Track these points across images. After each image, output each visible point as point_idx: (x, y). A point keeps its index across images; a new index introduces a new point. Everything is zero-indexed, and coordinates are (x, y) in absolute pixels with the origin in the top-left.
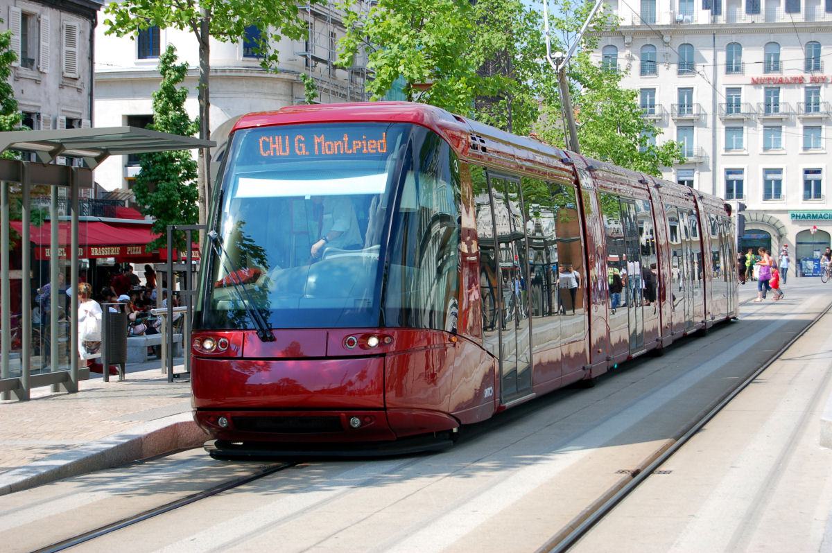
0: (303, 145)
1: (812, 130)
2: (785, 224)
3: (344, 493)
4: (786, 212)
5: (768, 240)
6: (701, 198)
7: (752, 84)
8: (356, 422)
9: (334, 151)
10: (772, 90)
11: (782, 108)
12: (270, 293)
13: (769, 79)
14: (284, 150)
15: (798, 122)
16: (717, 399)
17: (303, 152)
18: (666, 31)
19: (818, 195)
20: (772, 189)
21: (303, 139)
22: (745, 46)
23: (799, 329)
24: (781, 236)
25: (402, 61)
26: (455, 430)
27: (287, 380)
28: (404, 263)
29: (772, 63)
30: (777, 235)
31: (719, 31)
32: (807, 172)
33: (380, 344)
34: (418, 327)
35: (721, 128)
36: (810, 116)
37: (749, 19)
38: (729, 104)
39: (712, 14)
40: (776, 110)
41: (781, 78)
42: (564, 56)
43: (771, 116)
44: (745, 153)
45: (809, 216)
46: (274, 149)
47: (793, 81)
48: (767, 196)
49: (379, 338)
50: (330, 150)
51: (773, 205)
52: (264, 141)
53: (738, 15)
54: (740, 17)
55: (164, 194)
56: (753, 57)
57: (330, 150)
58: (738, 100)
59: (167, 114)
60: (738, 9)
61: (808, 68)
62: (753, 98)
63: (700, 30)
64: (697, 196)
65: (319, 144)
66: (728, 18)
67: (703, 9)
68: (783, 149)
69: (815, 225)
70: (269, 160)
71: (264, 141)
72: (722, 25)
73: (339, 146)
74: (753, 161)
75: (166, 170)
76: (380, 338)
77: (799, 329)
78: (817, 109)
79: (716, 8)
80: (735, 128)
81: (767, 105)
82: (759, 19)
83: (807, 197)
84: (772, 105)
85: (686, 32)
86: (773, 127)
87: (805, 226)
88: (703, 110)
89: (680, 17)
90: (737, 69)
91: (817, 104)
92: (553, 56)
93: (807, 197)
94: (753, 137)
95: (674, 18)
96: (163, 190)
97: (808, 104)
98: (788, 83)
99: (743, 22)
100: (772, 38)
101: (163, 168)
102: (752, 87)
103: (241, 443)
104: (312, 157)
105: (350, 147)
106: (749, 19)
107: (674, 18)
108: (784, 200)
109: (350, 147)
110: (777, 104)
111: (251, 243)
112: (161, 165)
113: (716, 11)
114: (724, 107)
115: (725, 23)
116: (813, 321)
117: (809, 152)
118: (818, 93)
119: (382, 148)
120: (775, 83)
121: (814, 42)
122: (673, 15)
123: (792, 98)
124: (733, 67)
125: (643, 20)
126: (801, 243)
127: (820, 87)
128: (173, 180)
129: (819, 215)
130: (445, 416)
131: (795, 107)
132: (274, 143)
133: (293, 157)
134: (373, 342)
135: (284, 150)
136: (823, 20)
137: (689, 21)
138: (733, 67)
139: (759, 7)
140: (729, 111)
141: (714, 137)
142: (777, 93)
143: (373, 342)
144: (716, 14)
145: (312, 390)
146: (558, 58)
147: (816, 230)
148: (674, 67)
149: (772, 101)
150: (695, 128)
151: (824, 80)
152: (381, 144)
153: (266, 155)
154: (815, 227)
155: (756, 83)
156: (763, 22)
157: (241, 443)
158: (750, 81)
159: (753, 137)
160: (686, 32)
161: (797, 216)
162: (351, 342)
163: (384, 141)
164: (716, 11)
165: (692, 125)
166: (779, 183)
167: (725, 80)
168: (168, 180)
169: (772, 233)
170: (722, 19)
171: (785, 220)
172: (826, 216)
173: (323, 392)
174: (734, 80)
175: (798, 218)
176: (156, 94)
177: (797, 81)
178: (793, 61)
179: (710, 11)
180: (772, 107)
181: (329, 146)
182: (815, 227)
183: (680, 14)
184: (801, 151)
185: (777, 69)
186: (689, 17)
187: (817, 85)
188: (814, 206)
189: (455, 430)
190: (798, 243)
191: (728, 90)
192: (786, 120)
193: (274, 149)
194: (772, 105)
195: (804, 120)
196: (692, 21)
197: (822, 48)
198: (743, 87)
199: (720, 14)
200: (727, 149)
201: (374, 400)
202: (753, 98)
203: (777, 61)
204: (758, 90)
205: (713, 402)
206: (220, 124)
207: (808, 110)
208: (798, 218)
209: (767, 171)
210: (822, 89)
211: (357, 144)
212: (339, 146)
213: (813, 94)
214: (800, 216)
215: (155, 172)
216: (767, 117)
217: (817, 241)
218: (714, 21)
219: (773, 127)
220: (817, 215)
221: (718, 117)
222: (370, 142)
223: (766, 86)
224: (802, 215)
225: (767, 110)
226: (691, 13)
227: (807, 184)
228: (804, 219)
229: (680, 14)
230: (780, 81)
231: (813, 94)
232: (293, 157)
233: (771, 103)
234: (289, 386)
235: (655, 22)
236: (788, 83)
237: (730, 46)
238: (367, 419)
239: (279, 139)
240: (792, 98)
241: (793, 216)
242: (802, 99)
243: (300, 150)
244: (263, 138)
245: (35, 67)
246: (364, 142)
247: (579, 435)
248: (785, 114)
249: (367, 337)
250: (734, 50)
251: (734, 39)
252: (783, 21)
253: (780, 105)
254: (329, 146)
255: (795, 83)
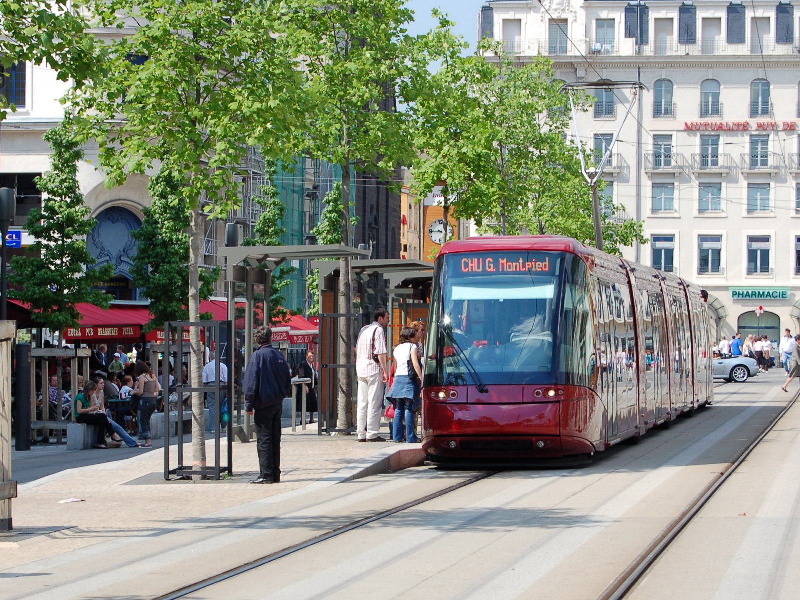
0: (492, 265)
1: (759, 188)
2: (725, 304)
3: (554, 482)
4: (726, 288)
6: (633, 270)
7: (685, 131)
8: (541, 444)
9: (513, 269)
10: (710, 139)
11: (721, 161)
13: (706, 125)
14: (479, 268)
15: (741, 178)
16: (743, 449)
17: (492, 270)
18: (580, 63)
19: (765, 268)
20: (709, 261)
21: (492, 261)
22: (678, 84)
23: (770, 418)
24: (720, 319)
25: (446, 170)
26: (592, 454)
27: (485, 417)
28: (566, 344)
29: (711, 106)
30: (714, 317)
31: (646, 65)
32: (752, 239)
33: (557, 395)
34: (574, 385)
35: (647, 184)
36: (756, 171)
37: (682, 50)
38: (657, 156)
39: (637, 44)
40: (715, 163)
41: (721, 124)
42: (597, 171)
43: (708, 171)
44: (677, 215)
45: (754, 294)
46: (472, 267)
47: (735, 128)
49: (555, 391)
50: (510, 268)
51: (709, 280)
52: (465, 262)
53: (668, 45)
54: (672, 49)
55: (166, 276)
56: (687, 101)
57: (510, 268)
58: (668, 150)
59: (166, 198)
60: (669, 38)
61: (754, 113)
62: (687, 148)
63: (623, 63)
64: (629, 269)
65: (503, 265)
66: (656, 49)
67: (626, 37)
68: (723, 211)
69: (761, 305)
70: (467, 274)
71: (465, 262)
72: (649, 58)
73: (516, 266)
74: (684, 223)
75: (167, 253)
76: (557, 391)
77: (770, 418)
78: (765, 163)
79: (641, 36)
80: (664, 185)
81: (704, 156)
82: (695, 50)
83: (751, 271)
84: (710, 156)
85: (606, 66)
86: (711, 187)
87: (748, 306)
88: (625, 161)
89: (598, 47)
90: (667, 112)
91: (765, 155)
92: (587, 171)
93: (751, 271)
94: (687, 195)
95: (591, 48)
96: (166, 273)
97: (754, 156)
98: (730, 130)
99: (674, 54)
100: (711, 74)
101: (164, 251)
102: (685, 134)
104: (498, 273)
105: (524, 266)
106: (682, 50)
107: (591, 48)
108: (723, 274)
109: (524, 266)
110: (715, 156)
112: (162, 248)
113: (642, 40)
114: (651, 158)
115: (652, 54)
116: (786, 408)
117: (755, 215)
118: (766, 143)
119: (546, 267)
120: (713, 130)
121: (762, 79)
122: (589, 44)
123: (733, 150)
124: (661, 110)
125: (552, 49)
126: (744, 328)
127: (769, 136)
128: (174, 263)
129: (766, 293)
130: (589, 444)
131: (738, 160)
132: (472, 263)
133: (485, 273)
134: (552, 393)
135: (479, 268)
136: (774, 54)
137: (608, 52)
138: (661, 110)
139: (695, 36)
140: (657, 164)
141: (639, 195)
142: (716, 143)
143: (552, 393)
144: (642, 43)
145: (501, 424)
146: (592, 173)
147: (762, 312)
148: (591, 110)
149: (710, 152)
150: (615, 184)
151: (774, 127)
152: (546, 265)
153: (466, 271)
154: (761, 308)
155: (690, 129)
156: (700, 54)
158: (683, 128)
159: (687, 195)
160: (606, 66)
161: (739, 294)
162: (538, 394)
163: (547, 264)
164: (642, 40)
165: (611, 180)
166: (718, 253)
167: (654, 125)
168: (169, 263)
170: (649, 50)
171: (725, 299)
172: (775, 295)
173: (507, 425)
174: (663, 125)
175: (741, 296)
176: (154, 178)
177: (741, 128)
178: (735, 103)
179: (634, 39)
180: (710, 159)
181: (510, 266)
182: (761, 308)
183: (597, 42)
184: (745, 214)
185: (716, 112)
186: (607, 47)
187: (765, 133)
188: (759, 282)
189: (592, 454)
190: (739, 328)
191: (656, 137)
192: (727, 175)
193: (472, 267)
194: (710, 156)
195: (748, 176)
196: (613, 52)
197: (772, 87)
198: (674, 134)
199: (647, 43)
200: (654, 211)
201: (554, 431)
202: (687, 148)
203: (716, 103)
204: (692, 138)
205: (740, 452)
206: (95, 185)
207: (754, 163)
208: (741, 296)
209: (703, 238)
210: (771, 138)
211: (529, 265)
212: (516, 266)
213: (760, 144)
214: (743, 295)
215: (154, 255)
216: (703, 171)
217: (763, 326)
218: (639, 52)
219: (711, 187)
220: (764, 293)
221: (643, 171)
222: (538, 264)
223: (703, 133)
224: (745, 293)
225: (704, 163)
226: (612, 41)
227: (752, 255)
228: (748, 298)
229: (597, 42)
230: (721, 128)
231: (760, 144)
232: (485, 273)
233: (709, 156)
234: (487, 422)
235: (566, 52)
236: (730, 130)
237: (659, 83)
238: (549, 442)
239: (475, 260)
240: (733, 150)
241: (735, 294)
242: (747, 150)
243: (490, 268)
244: (464, 260)
246: (534, 264)
247: (670, 459)
248: (727, 168)
249: (549, 390)
250: (663, 88)
251: (664, 74)
252: (724, 54)
253: (719, 156)
254: (510, 266)
255: (738, 130)
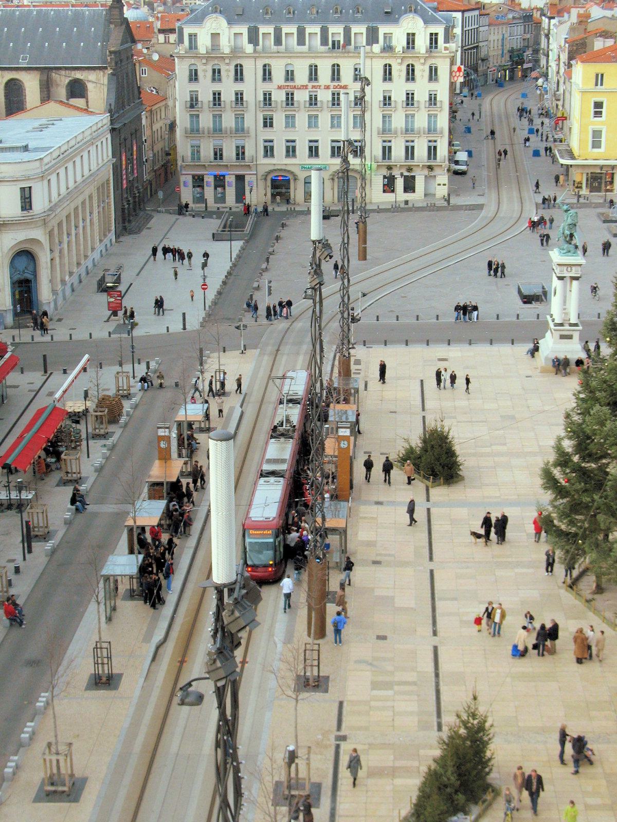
5: (289, 181)
12: (541, 514)
19: (317, 155)
48: (288, 155)
74: (279, 135)
103: (87, 356)
106: (274, 48)
111: (553, 294)
157: (87, 356)
169: (291, 177)
170: (260, 48)
174: (268, 87)
185: (292, 79)
245: (233, 586)
